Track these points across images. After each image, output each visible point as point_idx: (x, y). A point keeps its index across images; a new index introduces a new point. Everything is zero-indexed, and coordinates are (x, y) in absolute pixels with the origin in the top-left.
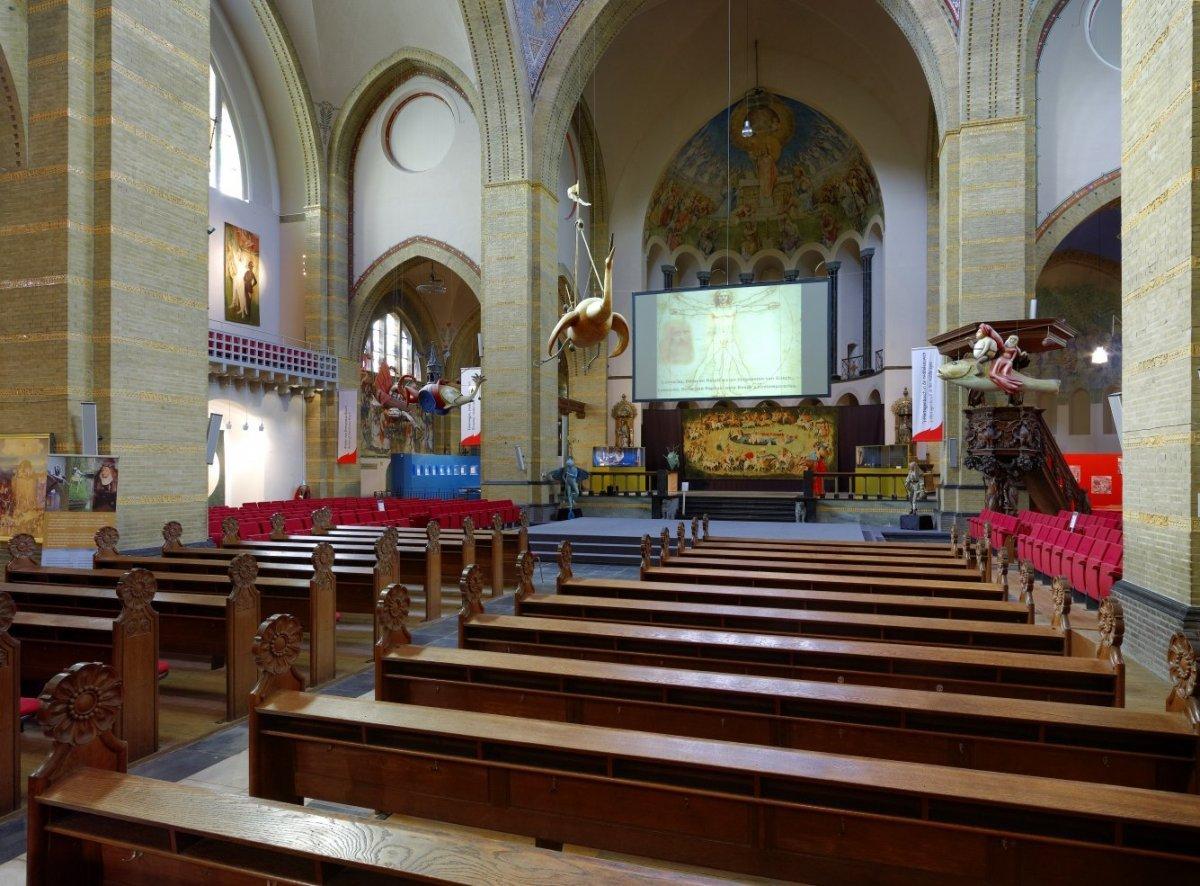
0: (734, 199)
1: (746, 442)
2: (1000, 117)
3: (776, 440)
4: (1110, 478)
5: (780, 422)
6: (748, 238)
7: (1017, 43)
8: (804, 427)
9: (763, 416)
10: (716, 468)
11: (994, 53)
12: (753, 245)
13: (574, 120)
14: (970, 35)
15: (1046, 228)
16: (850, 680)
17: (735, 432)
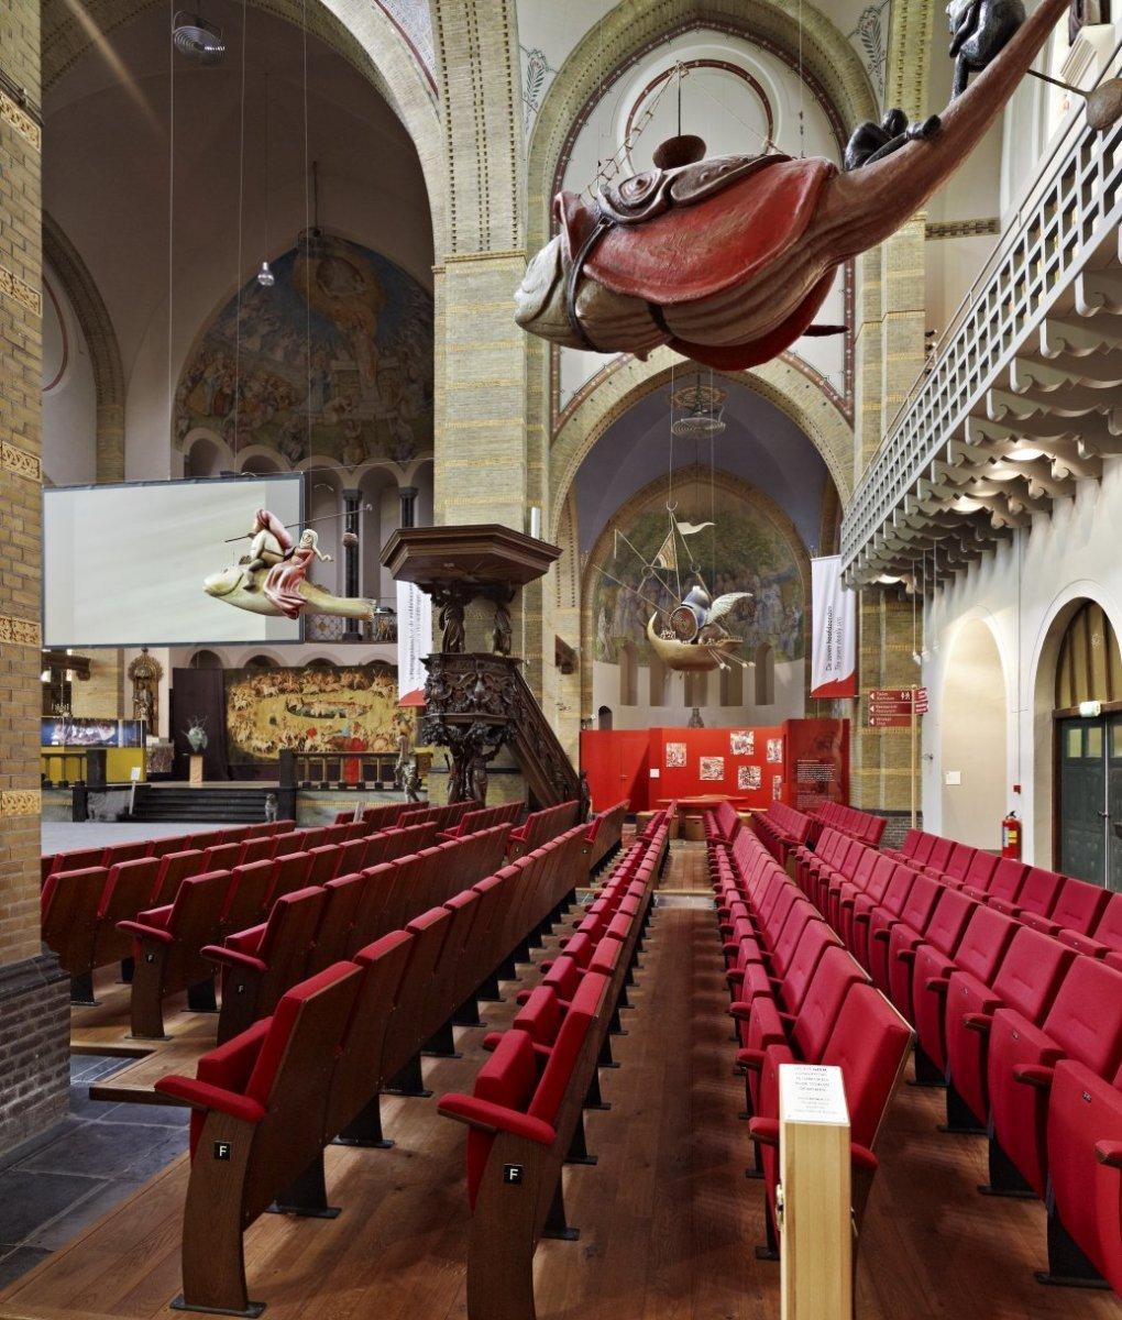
0: (327, 386)
1: (308, 714)
2: (495, 249)
3: (346, 712)
4: (721, 759)
5: (351, 686)
6: (351, 441)
7: (510, 146)
8: (380, 694)
9: (330, 679)
10: (269, 750)
11: (482, 157)
12: (358, 451)
13: (46, 250)
14: (450, 129)
15: (571, 413)
16: (24, 1043)
17: (294, 700)
